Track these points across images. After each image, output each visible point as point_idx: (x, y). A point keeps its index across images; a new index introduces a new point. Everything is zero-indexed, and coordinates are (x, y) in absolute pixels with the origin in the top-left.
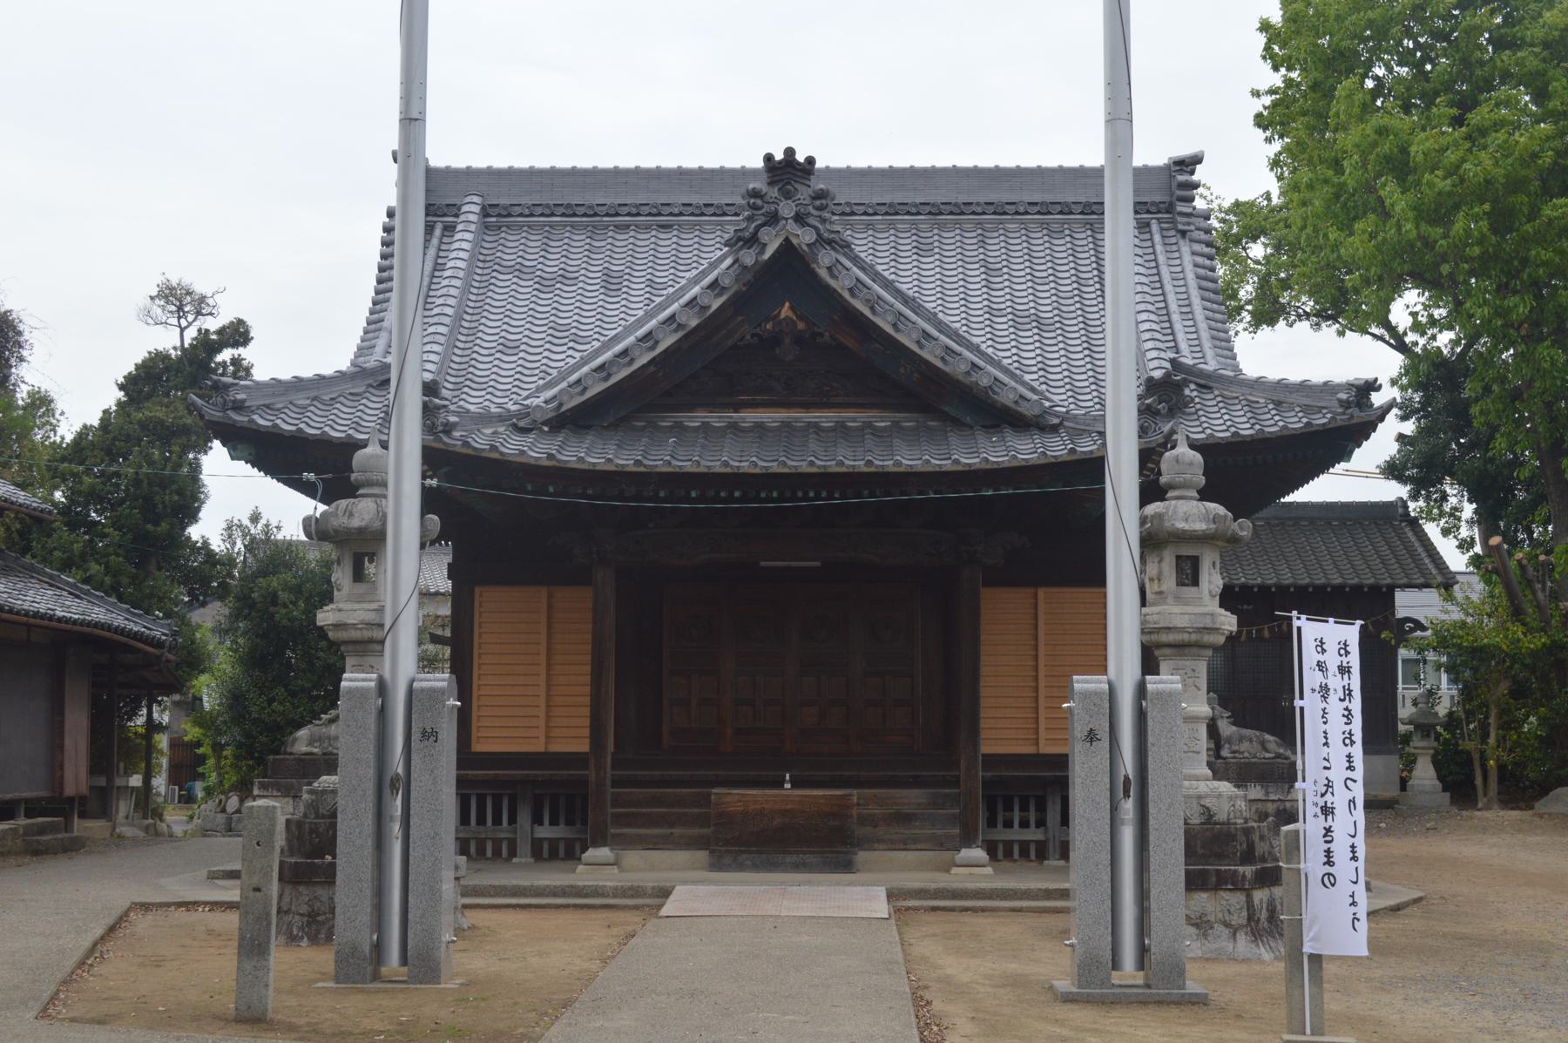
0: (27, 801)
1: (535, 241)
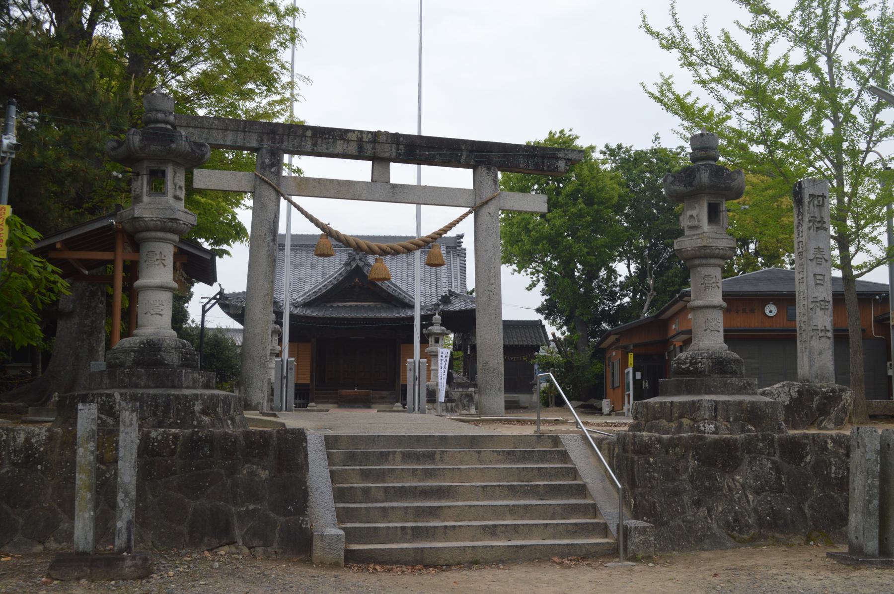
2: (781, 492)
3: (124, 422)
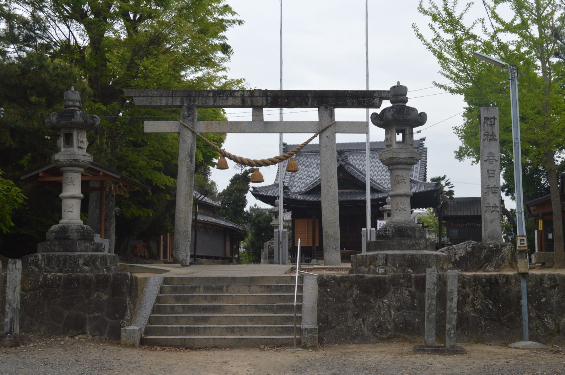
1: (305, 158)
2: (415, 310)
3: (9, 269)
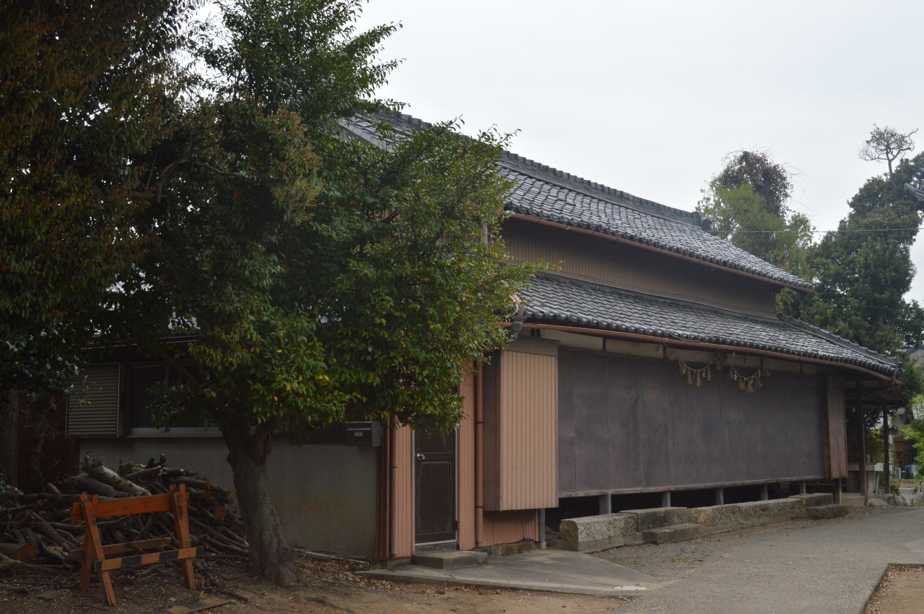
0: (807, 481)
